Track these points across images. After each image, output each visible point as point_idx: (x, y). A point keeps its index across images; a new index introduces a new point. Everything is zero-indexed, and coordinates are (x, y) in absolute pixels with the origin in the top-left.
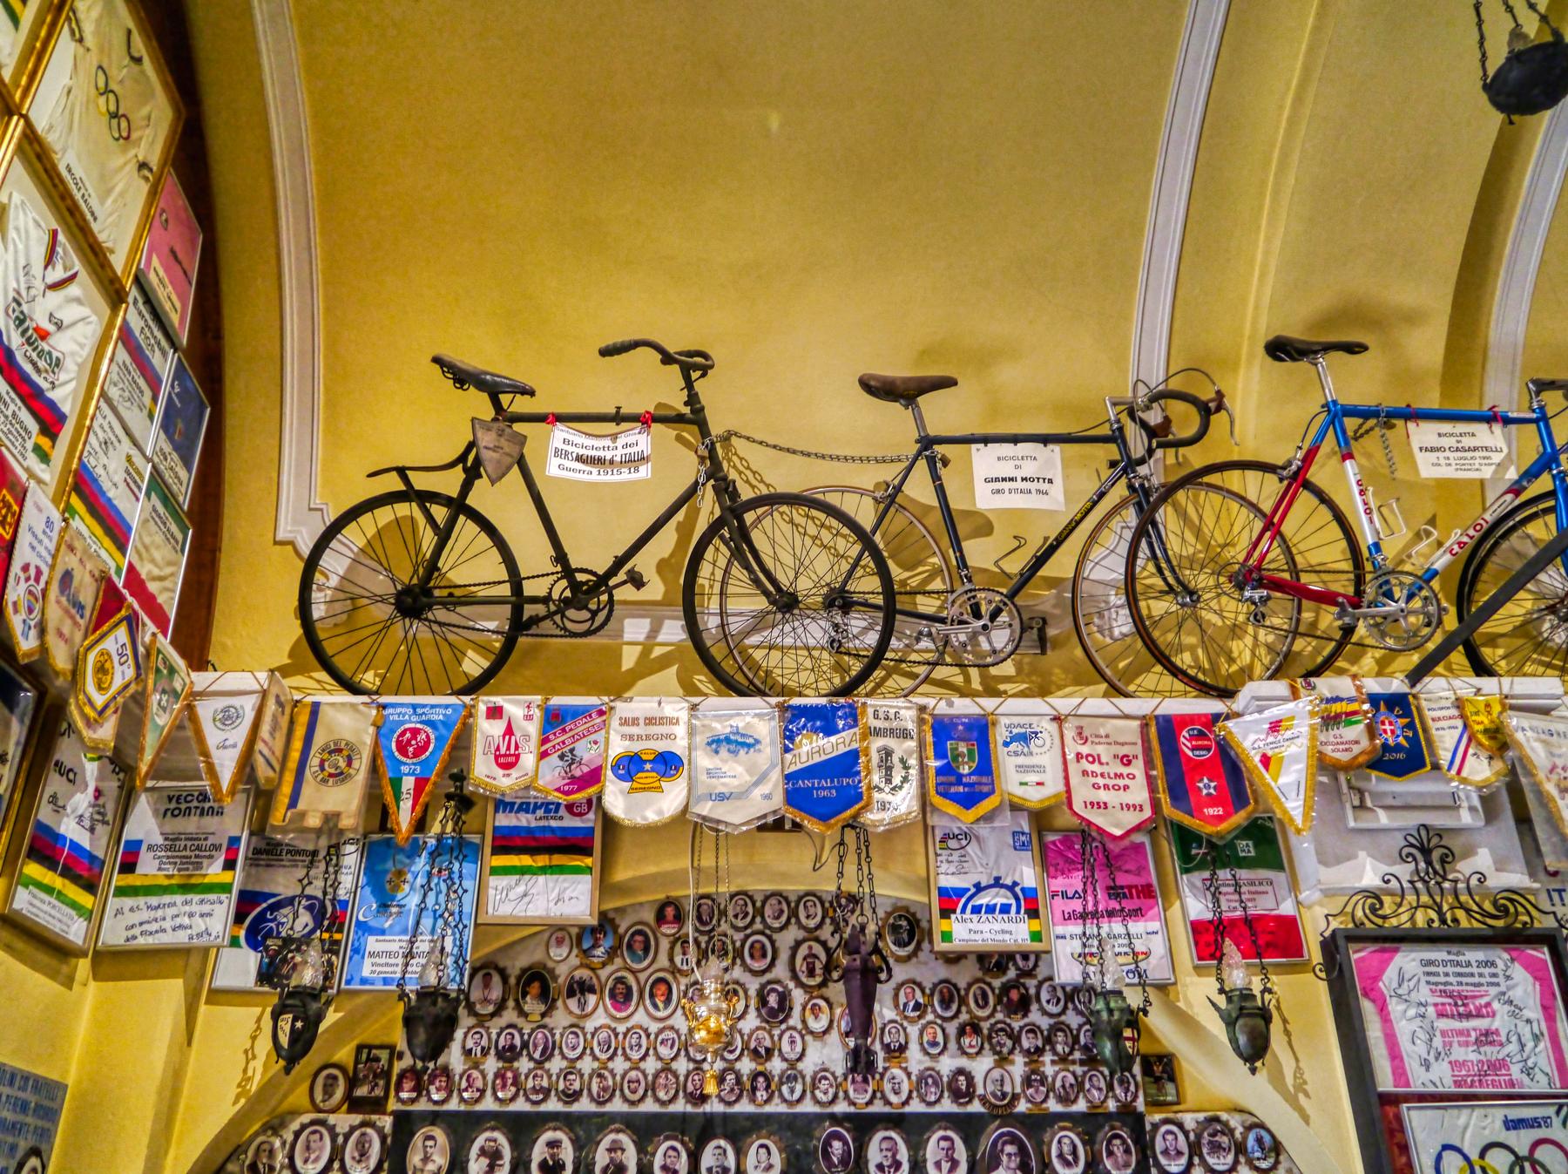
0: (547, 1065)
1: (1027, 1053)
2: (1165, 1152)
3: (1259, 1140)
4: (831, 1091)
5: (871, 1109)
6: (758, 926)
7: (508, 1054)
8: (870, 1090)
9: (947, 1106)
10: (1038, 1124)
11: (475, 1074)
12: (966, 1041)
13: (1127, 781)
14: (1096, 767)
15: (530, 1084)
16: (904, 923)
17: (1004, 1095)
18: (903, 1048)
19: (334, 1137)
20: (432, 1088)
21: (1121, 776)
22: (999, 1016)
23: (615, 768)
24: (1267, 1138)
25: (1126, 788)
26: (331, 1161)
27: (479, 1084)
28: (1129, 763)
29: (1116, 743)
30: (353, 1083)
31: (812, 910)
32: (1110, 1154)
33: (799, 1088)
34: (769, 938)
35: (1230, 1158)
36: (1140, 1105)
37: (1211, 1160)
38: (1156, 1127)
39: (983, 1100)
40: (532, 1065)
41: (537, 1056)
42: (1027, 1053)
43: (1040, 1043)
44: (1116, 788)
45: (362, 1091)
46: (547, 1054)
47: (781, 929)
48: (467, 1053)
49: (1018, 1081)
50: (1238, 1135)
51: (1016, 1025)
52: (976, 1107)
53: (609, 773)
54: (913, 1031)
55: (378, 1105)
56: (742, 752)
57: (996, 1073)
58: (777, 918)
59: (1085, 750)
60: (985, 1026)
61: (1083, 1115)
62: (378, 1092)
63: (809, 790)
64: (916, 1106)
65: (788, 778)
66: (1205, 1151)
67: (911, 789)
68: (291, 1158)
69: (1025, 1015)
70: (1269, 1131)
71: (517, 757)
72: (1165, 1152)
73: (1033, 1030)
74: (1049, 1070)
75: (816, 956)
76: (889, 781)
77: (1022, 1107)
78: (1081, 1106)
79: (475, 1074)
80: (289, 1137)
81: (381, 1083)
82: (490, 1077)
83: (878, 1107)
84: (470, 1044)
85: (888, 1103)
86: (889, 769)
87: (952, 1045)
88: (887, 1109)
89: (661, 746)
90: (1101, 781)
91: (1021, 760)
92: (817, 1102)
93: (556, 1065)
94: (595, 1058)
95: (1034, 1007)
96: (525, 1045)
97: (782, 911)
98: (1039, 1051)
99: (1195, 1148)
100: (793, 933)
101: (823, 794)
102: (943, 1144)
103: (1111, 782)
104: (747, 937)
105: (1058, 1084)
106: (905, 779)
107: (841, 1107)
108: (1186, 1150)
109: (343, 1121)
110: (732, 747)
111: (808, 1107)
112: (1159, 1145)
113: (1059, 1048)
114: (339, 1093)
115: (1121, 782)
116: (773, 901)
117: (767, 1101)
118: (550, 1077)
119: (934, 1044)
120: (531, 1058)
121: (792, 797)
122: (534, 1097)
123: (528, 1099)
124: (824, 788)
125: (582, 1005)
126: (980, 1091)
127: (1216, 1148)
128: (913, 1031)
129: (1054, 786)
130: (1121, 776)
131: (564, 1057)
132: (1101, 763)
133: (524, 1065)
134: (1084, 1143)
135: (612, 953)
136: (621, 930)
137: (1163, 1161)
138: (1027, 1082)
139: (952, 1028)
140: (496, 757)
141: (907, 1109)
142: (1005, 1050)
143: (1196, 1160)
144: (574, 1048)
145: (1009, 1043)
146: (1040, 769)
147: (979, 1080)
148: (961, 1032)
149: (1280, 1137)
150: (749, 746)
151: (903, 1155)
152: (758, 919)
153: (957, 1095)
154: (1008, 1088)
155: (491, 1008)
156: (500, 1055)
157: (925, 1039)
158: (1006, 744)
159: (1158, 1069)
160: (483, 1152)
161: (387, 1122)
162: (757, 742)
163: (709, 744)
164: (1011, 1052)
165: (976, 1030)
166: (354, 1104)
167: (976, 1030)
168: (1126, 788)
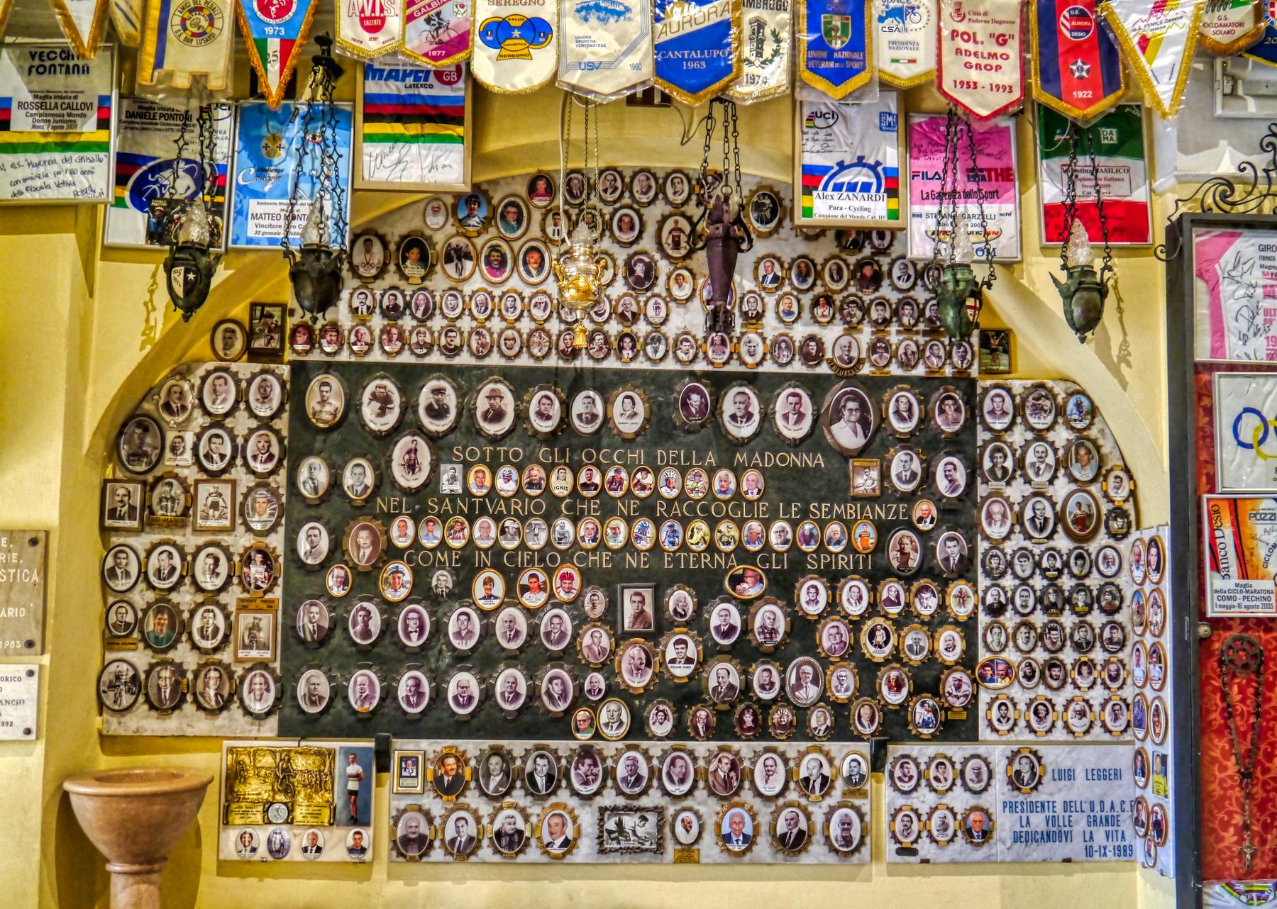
0: (429, 323)
2: (992, 412)
3: (1079, 405)
4: (692, 352)
5: (727, 368)
6: (627, 200)
7: (393, 313)
8: (728, 352)
9: (798, 367)
10: (879, 385)
11: (363, 329)
12: (819, 311)
13: (999, 62)
14: (970, 46)
15: (414, 339)
16: (767, 201)
17: (851, 360)
18: (759, 316)
19: (237, 382)
20: (324, 342)
21: (994, 56)
22: (852, 290)
23: (483, 35)
24: (1086, 403)
25: (998, 68)
26: (237, 402)
27: (367, 338)
28: (1005, 42)
29: (994, 21)
30: (250, 336)
31: (679, 187)
32: (942, 411)
33: (662, 348)
34: (637, 212)
35: (1050, 419)
36: (974, 371)
37: (1032, 420)
38: (986, 390)
39: (831, 363)
40: (415, 323)
41: (419, 314)
43: (888, 315)
44: (988, 68)
45: (259, 343)
46: (429, 314)
47: (649, 204)
48: (355, 311)
49: (864, 347)
50: (1060, 400)
51: (867, 299)
52: (824, 369)
53: (477, 38)
54: (770, 301)
55: (275, 356)
56: (612, 20)
57: (845, 341)
58: (645, 193)
59: (961, 27)
60: (838, 298)
61: (921, 379)
62: (275, 344)
63: (679, 61)
64: (769, 367)
65: (658, 48)
66: (1028, 412)
67: (782, 62)
68: (201, 399)
69: (876, 290)
70: (1088, 398)
71: (383, 19)
72: (992, 412)
73: (882, 303)
74: (894, 339)
75: (681, 230)
76: (759, 54)
78: (920, 371)
79: (363, 329)
80: (197, 382)
81: (276, 336)
82: (377, 333)
83: (734, 367)
84: (356, 303)
85: (743, 363)
86: (761, 42)
87: (806, 314)
88: (743, 369)
89: (530, 11)
90: (973, 60)
91: (896, 36)
92: (679, 361)
93: (437, 323)
94: (474, 318)
95: (886, 283)
96: (408, 305)
97: (650, 187)
98: (886, 322)
99: (1019, 410)
100: (660, 208)
101: (692, 65)
102: (792, 399)
103: (983, 62)
104: (616, 211)
105: (901, 351)
106: (776, 53)
107: (701, 366)
108: (1011, 412)
109: (245, 369)
110: (602, 15)
111: (670, 365)
112: (987, 405)
113: (905, 320)
114: (239, 344)
115: (994, 62)
116: (641, 177)
117: (632, 359)
118: (432, 334)
119: (789, 313)
120: (414, 317)
121: (662, 69)
122: (418, 351)
123: (413, 353)
124: (694, 60)
125: (460, 270)
126: (829, 355)
127: (1038, 410)
128: (770, 301)
129: (925, 63)
130: (994, 56)
131: (444, 317)
132: (975, 42)
133: (407, 322)
134: (920, 403)
135: (487, 222)
136: (495, 202)
137: (989, 419)
138: (873, 348)
139: (807, 300)
140: (362, 20)
141: (760, 369)
142: (855, 320)
143: (1019, 420)
144: (453, 309)
145: (859, 314)
146: (913, 45)
147: (828, 345)
148: (816, 303)
149: (1097, 403)
150: (619, 14)
151: (755, 407)
152: (627, 194)
153: (807, 358)
154: (854, 354)
155: (374, 272)
156: (385, 313)
157: (781, 308)
158: (881, 19)
159: (994, 342)
160: (374, 397)
161: (285, 371)
162: (628, 9)
163: (578, 11)
164: (860, 322)
165: (829, 301)
166: (254, 355)
167: (829, 301)
168: (998, 68)
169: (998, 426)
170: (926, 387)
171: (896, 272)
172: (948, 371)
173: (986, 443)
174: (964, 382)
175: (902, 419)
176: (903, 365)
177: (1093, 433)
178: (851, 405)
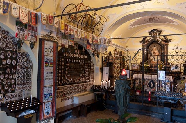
1: (6, 43)
10: (7, 51)
37: (23, 57)
42: (6, 43)
57: (2, 45)
74: (8, 46)
77: (5, 49)
78: (11, 50)
95: (8, 39)
99: (22, 55)
112: (19, 54)
127: (24, 55)
138: (6, 46)
154: (3, 47)
169: (19, 57)
170: (12, 52)
171: (9, 38)
172: (14, 50)
173: (18, 59)
174: (16, 51)
175: (9, 55)
176: (9, 49)
177: (29, 58)
178: (3, 53)
